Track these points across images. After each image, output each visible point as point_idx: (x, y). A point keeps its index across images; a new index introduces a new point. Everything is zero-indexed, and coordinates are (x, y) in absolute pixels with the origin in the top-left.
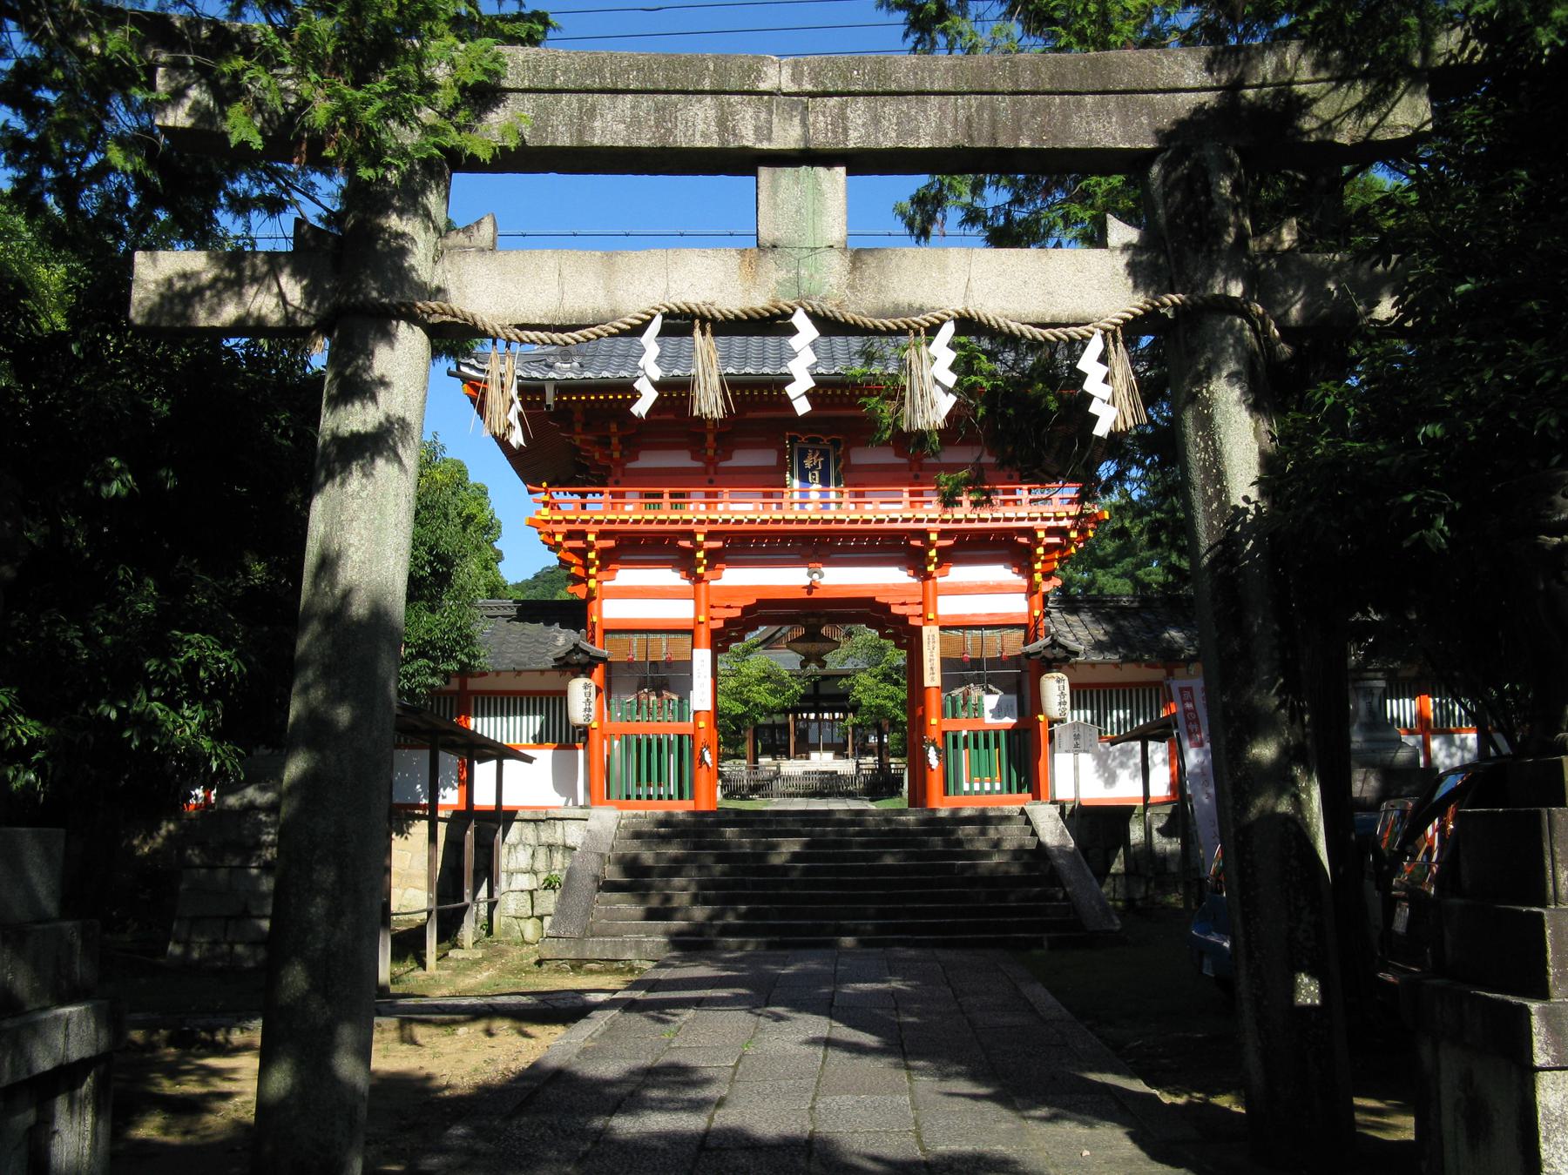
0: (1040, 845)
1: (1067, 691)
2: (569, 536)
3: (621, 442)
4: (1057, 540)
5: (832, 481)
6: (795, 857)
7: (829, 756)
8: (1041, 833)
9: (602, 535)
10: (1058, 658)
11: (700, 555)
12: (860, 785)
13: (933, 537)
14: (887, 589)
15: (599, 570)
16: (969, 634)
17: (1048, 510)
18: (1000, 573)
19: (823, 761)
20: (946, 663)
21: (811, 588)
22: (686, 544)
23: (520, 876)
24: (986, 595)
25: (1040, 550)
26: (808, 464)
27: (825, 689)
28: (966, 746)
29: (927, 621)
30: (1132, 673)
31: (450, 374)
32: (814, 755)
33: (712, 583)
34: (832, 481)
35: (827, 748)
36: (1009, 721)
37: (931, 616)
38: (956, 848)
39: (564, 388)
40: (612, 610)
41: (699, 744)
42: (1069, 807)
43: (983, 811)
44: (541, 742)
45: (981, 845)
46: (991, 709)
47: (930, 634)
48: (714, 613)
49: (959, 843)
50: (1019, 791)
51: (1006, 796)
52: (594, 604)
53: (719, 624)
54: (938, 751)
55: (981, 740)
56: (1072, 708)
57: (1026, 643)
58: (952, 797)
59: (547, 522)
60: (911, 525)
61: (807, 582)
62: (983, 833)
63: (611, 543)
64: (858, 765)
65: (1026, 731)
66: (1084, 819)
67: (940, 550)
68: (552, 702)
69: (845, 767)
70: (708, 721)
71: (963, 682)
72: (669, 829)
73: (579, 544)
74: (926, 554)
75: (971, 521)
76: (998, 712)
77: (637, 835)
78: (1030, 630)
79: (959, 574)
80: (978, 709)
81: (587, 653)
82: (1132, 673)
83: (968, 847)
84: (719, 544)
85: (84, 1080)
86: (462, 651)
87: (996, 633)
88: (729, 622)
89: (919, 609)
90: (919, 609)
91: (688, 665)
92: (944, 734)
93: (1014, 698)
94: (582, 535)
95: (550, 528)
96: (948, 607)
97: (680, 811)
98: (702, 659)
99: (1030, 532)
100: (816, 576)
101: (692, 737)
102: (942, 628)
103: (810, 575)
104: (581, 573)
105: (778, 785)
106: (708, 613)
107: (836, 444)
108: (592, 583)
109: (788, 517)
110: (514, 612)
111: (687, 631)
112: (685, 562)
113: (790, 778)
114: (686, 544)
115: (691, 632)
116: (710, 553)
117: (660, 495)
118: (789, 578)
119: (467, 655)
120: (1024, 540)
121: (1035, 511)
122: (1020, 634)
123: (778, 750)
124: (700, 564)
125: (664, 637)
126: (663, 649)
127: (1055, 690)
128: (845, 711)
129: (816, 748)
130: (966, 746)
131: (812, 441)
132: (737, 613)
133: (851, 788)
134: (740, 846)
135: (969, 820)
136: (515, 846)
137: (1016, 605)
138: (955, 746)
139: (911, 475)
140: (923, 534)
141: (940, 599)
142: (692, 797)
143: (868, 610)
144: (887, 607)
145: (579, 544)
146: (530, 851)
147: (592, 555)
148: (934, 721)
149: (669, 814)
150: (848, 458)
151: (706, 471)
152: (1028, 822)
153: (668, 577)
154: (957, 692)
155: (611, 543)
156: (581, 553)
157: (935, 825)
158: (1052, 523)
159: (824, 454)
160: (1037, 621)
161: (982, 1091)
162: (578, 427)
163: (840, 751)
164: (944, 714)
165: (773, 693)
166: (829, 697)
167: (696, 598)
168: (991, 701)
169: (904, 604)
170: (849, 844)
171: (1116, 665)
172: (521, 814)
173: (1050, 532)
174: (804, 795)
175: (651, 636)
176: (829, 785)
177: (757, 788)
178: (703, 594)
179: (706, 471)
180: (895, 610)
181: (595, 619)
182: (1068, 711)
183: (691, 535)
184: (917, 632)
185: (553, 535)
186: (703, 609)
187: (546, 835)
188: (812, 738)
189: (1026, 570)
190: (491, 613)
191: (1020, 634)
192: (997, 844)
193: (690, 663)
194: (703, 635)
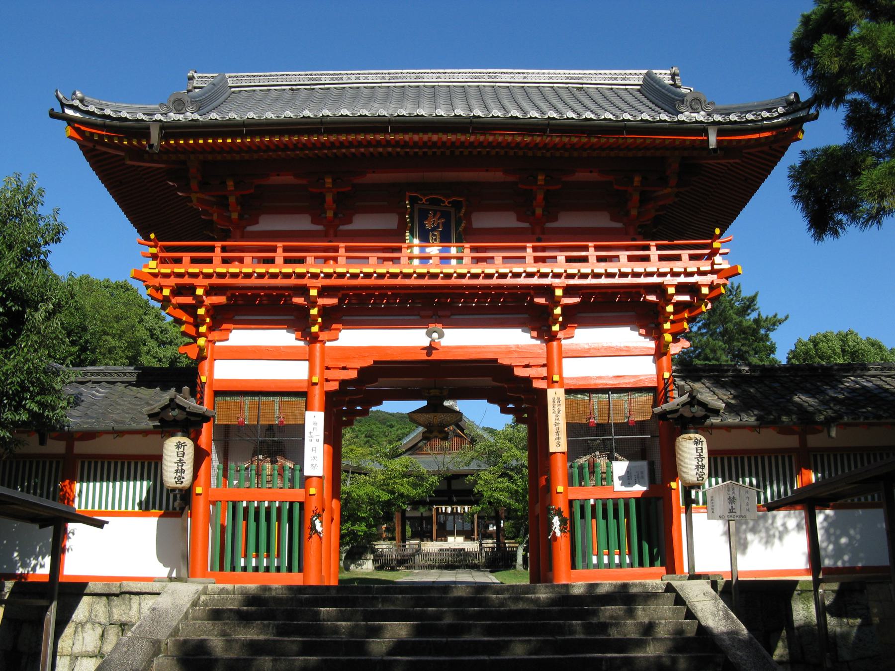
0: (703, 631)
1: (705, 454)
2: (178, 291)
4: (686, 298)
5: (453, 237)
6: (400, 647)
7: (460, 539)
8: (700, 615)
10: (693, 419)
12: (482, 560)
13: (559, 292)
14: (508, 351)
15: (211, 329)
16: (597, 399)
17: (678, 267)
18: (625, 336)
19: (456, 542)
20: (572, 429)
21: (430, 349)
22: (299, 300)
24: (613, 358)
25: (670, 309)
26: (428, 227)
27: (456, 485)
28: (594, 516)
29: (552, 383)
30: (770, 439)
31: (53, 115)
32: (450, 539)
33: (328, 344)
34: (453, 237)
35: (459, 534)
36: (639, 489)
37: (556, 378)
38: (600, 638)
39: (170, 130)
40: (225, 371)
41: (309, 514)
42: (721, 583)
43: (625, 586)
44: (147, 509)
45: (630, 629)
46: (620, 478)
47: (555, 396)
48: (330, 374)
49: (604, 627)
50: (652, 565)
51: (637, 569)
52: (206, 364)
53: (335, 386)
54: (563, 522)
55: (610, 509)
56: (710, 476)
57: (654, 406)
58: (580, 571)
59: (155, 275)
60: (535, 281)
61: (426, 342)
62: (631, 613)
63: (222, 299)
64: (481, 544)
65: (658, 499)
66: (742, 594)
67: (565, 308)
68: (149, 465)
69: (472, 546)
70: (321, 489)
71: (587, 449)
72: (257, 607)
73: (189, 300)
74: (551, 313)
75: (597, 276)
76: (627, 479)
77: (216, 615)
78: (658, 393)
79: (584, 336)
80: (607, 477)
81: (182, 408)
82: (770, 439)
83: (614, 634)
84: (334, 301)
86: (32, 399)
87: (624, 397)
89: (543, 372)
90: (543, 372)
91: (300, 429)
92: (571, 502)
93: (644, 464)
94: (189, 290)
95: (159, 281)
96: (574, 370)
97: (275, 586)
98: (315, 423)
99: (659, 289)
100: (435, 335)
101: (302, 505)
102: (568, 392)
103: (429, 334)
104: (192, 331)
105: (419, 559)
106: (322, 374)
107: (457, 205)
108: (201, 341)
109: (405, 271)
110: (133, 379)
111: (298, 394)
112: (298, 321)
113: (428, 554)
114: (299, 300)
115: (303, 394)
116: (325, 311)
118: (408, 339)
119: (40, 404)
120: (652, 298)
122: (648, 397)
123: (424, 535)
124: (315, 323)
125: (277, 400)
126: (276, 412)
127: (692, 452)
128: (470, 503)
129: (451, 534)
130: (594, 516)
131: (435, 202)
132: (353, 374)
133: (476, 562)
134: (336, 631)
135: (609, 599)
136: (82, 625)
137: (644, 369)
138: (583, 516)
140: (548, 291)
141: (565, 361)
142: (300, 570)
144: (510, 368)
145: (189, 300)
146: (99, 630)
147: (201, 311)
148: (560, 489)
149: (266, 589)
150: (469, 222)
152: (679, 600)
153: (283, 338)
154: (582, 460)
155: (222, 299)
156: (190, 309)
157: (571, 605)
158: (682, 279)
159: (445, 215)
160: (666, 382)
162: (194, 184)
163: (468, 536)
164: (570, 482)
165: (414, 486)
166: (459, 493)
167: (310, 359)
168: (620, 467)
171: (751, 428)
172: (92, 587)
173: (681, 289)
174: (440, 567)
175: (264, 399)
176: (459, 560)
177: (404, 562)
178: (318, 354)
179: (323, 236)
180: (518, 372)
182: (706, 476)
183: (303, 291)
185: (160, 289)
186: (318, 370)
187: (119, 612)
188: (449, 527)
189: (654, 330)
190: (109, 379)
191: (648, 397)
192: (649, 629)
193: (302, 426)
194: (317, 396)
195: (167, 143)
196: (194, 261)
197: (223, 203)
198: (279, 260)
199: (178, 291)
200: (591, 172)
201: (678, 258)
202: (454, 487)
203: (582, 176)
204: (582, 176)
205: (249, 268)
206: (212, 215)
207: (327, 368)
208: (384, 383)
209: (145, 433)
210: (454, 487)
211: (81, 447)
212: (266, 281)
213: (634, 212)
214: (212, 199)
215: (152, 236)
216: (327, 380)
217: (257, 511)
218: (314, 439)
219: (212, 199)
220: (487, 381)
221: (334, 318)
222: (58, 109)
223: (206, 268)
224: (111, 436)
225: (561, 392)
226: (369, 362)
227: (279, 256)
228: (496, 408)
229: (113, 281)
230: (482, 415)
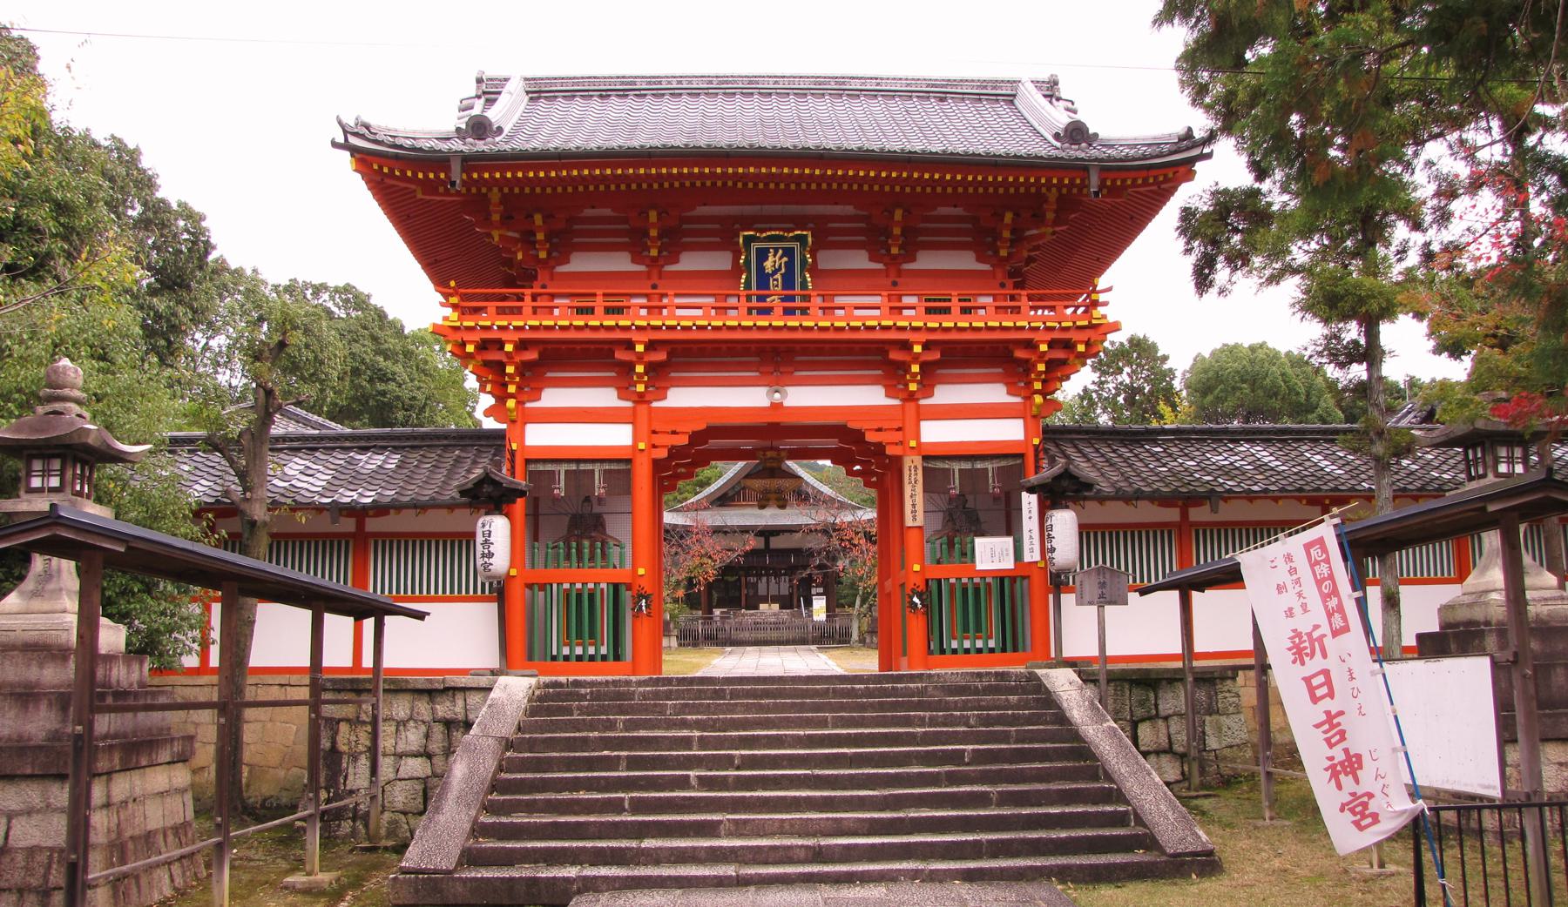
3: (548, 238)
9: (522, 345)
11: (640, 369)
23: (411, 761)
31: (335, 145)
35: (774, 600)
48: (658, 439)
53: (662, 454)
88: (675, 452)
89: (898, 436)
90: (898, 436)
96: (935, 432)
101: (930, 652)
102: (925, 458)
106: (649, 439)
112: (622, 376)
114: (621, 355)
117: (595, 295)
118: (745, 398)
132: (683, 440)
139: (888, 282)
143: (847, 442)
144: (859, 435)
146: (423, 728)
151: (648, 275)
153: (606, 397)
158: (1056, 335)
161: (135, 890)
169: (880, 430)
180: (871, 437)
181: (514, 446)
183: (1030, 345)
184: (897, 462)
185: (464, 344)
195: (469, 177)
196: (501, 312)
197: (528, 240)
198: (599, 311)
199: (483, 346)
202: (772, 546)
203: (944, 211)
204: (944, 211)
205: (560, 318)
206: (515, 253)
207: (654, 432)
208: (714, 443)
209: (451, 506)
210: (772, 546)
211: (373, 525)
212: (588, 335)
213: (1003, 253)
214: (516, 235)
215: (453, 284)
216: (654, 446)
217: (579, 595)
219: (516, 235)
220: (832, 443)
221: (660, 376)
222: (341, 139)
224: (413, 512)
225: (918, 460)
226: (702, 426)
227: (599, 303)
229: (145, 163)
230: (818, 474)
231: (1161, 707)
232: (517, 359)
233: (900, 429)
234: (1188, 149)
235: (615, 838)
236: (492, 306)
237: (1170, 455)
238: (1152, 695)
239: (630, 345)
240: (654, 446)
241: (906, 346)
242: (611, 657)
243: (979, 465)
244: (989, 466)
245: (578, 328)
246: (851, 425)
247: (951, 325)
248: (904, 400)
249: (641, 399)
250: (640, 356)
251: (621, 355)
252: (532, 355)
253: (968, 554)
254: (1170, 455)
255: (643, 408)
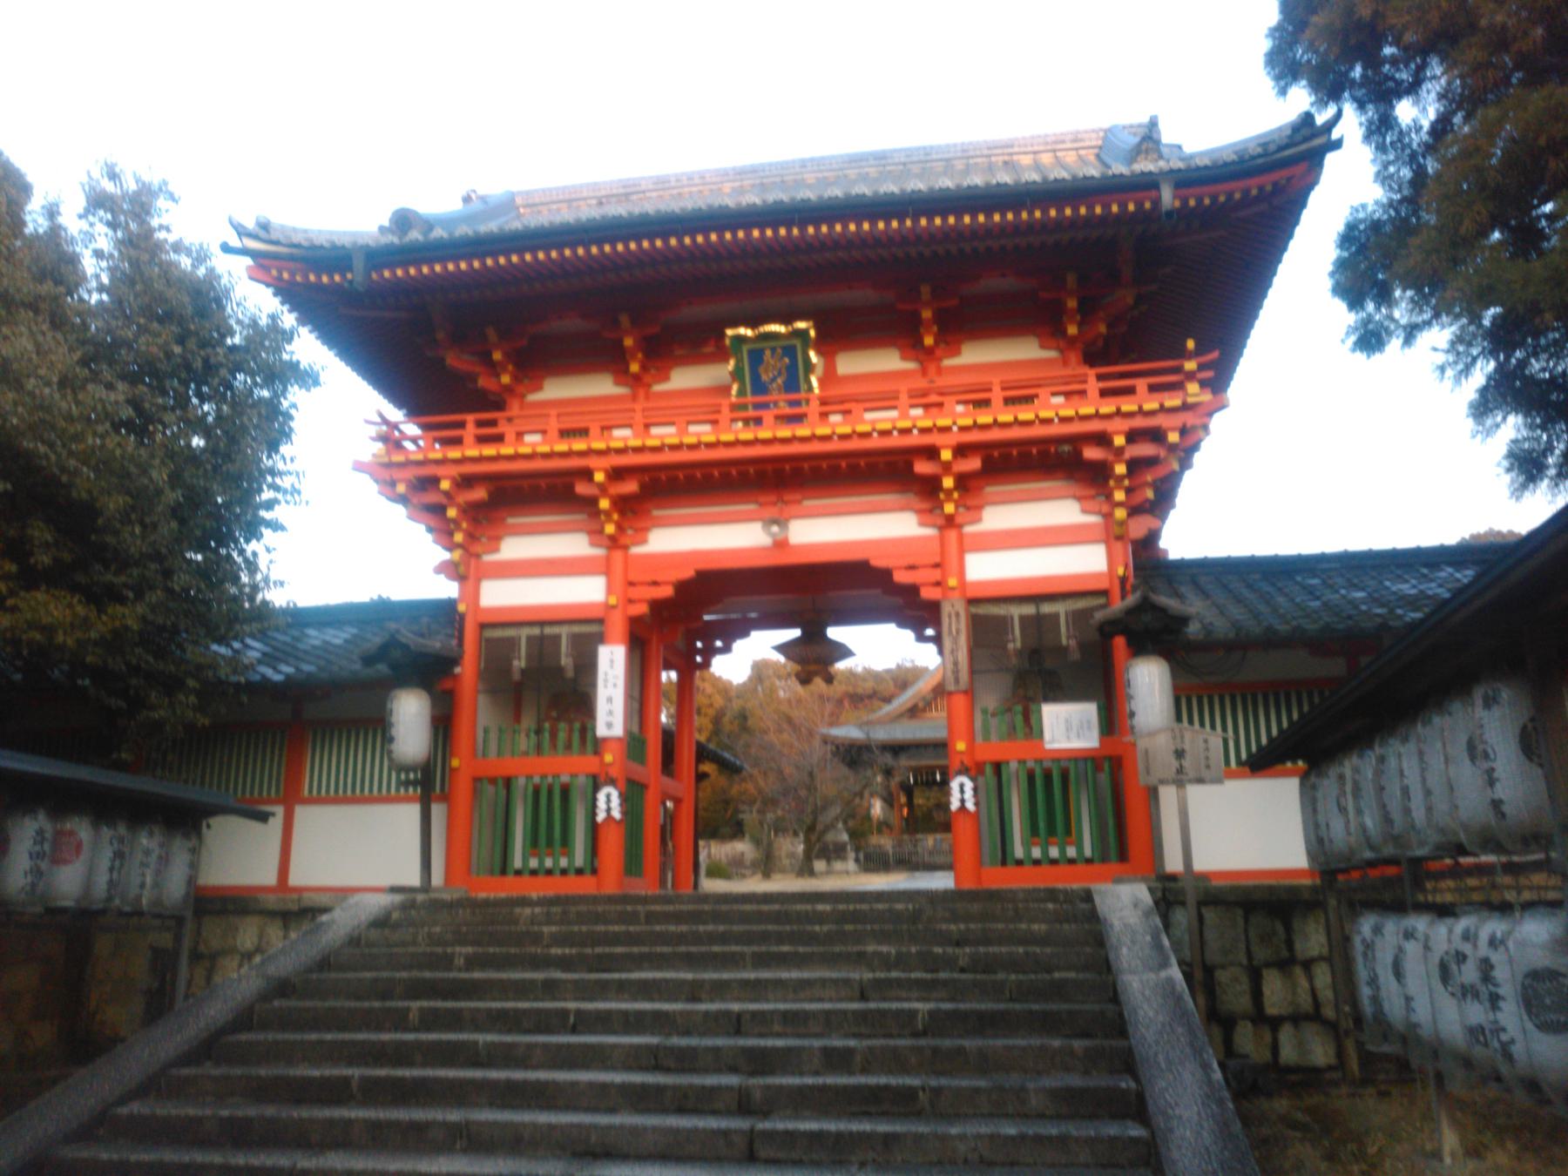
9: (961, 451)
18: (1063, 510)
48: (635, 593)
53: (642, 609)
85: (131, 1117)
89: (936, 575)
90: (936, 575)
96: (984, 568)
98: (612, 661)
112: (929, 489)
116: (963, 481)
121: (1107, 408)
132: (667, 592)
144: (886, 574)
153: (574, 545)
158: (1139, 422)
170: (536, 939)
180: (901, 577)
183: (1103, 439)
194: (618, 625)
200: (1004, 275)
201: (1130, 391)
207: (631, 584)
216: (631, 601)
218: (610, 685)
222: (235, 242)
223: (1171, 398)
225: (960, 607)
226: (688, 573)
228: (908, 635)
231: (1298, 946)
232: (1127, 456)
233: (937, 566)
234: (1306, 139)
235: (845, 1088)
236: (1141, 384)
237: (1331, 587)
238: (1280, 928)
239: (587, 474)
240: (631, 601)
241: (931, 453)
242: (588, 870)
243: (1047, 608)
244: (1060, 608)
245: (784, 441)
246: (875, 562)
247: (1134, 408)
248: (941, 528)
249: (614, 543)
250: (603, 489)
251: (922, 467)
252: (631, 487)
253: (1032, 727)
254: (1331, 587)
255: (618, 555)
